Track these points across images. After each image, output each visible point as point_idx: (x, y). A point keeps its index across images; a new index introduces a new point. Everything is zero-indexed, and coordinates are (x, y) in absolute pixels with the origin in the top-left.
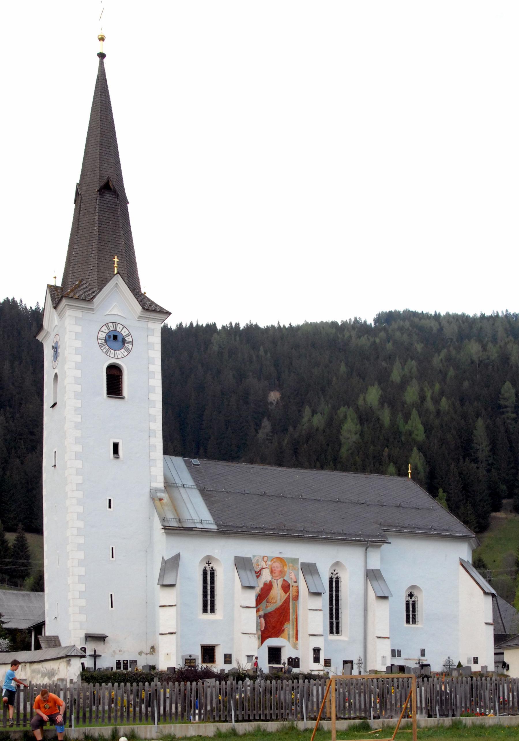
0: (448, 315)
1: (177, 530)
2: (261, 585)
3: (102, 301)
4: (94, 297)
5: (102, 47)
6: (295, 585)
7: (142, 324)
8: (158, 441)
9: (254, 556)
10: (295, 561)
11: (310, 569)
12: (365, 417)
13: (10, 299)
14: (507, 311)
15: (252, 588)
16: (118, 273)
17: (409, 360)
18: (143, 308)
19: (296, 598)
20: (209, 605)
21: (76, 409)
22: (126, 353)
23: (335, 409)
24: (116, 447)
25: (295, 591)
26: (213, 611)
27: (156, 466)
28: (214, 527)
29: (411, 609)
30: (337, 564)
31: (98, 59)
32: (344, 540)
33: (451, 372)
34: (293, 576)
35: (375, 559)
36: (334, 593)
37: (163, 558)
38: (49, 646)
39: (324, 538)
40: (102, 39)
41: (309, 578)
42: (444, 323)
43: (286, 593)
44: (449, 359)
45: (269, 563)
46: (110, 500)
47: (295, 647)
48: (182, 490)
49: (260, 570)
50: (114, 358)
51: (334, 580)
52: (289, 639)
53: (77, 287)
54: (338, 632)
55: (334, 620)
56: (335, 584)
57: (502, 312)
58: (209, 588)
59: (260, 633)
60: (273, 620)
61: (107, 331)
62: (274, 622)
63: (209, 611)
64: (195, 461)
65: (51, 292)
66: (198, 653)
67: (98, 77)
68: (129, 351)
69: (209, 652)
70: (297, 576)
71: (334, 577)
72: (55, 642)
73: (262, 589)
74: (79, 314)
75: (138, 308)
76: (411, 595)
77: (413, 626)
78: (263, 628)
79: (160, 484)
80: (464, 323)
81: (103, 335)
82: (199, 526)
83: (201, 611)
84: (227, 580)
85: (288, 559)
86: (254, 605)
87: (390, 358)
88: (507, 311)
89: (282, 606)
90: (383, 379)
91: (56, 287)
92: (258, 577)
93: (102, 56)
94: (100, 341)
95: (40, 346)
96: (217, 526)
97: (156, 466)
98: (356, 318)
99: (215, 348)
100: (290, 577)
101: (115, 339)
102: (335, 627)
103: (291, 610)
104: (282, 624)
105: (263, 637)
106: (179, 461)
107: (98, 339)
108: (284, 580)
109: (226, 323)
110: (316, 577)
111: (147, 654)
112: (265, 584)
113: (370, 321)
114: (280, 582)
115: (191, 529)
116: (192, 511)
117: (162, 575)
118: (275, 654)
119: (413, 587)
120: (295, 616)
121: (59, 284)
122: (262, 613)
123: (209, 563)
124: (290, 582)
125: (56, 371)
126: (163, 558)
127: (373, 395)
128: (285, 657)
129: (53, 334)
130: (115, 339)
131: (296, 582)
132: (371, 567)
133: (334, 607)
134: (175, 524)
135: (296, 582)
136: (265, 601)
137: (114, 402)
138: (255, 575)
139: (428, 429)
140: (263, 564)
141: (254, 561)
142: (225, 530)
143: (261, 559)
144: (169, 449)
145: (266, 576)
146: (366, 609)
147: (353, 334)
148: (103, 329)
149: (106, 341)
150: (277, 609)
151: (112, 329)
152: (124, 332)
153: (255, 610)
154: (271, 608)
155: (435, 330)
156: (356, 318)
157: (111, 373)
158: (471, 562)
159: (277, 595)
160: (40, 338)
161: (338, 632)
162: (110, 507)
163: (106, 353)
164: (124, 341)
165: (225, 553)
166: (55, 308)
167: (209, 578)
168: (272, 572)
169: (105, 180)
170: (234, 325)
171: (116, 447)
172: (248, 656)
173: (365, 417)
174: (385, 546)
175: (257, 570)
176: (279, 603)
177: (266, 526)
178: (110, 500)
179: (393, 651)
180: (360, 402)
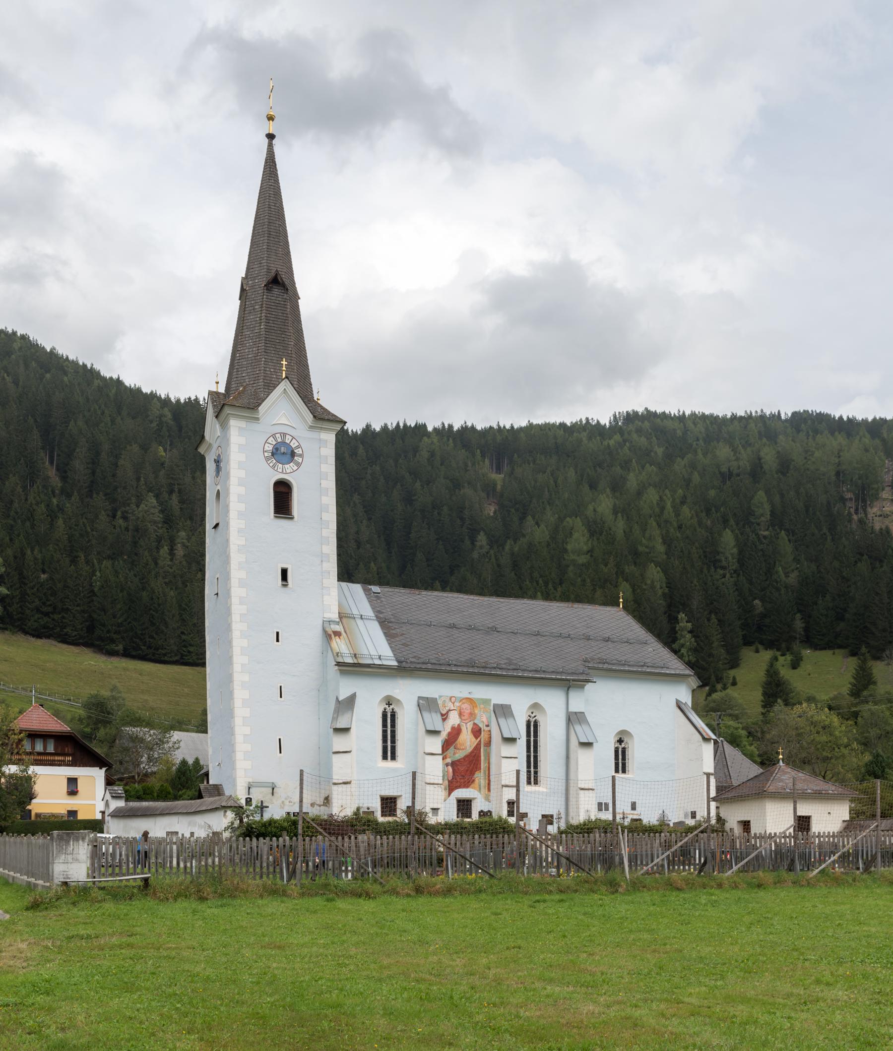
0: (693, 414)
1: (354, 668)
2: (448, 729)
3: (266, 411)
4: (260, 405)
5: (272, 128)
6: (487, 729)
7: (314, 435)
8: (332, 566)
9: (440, 697)
10: (487, 702)
11: (503, 711)
12: (596, 529)
13: (193, 398)
14: (762, 411)
15: (435, 733)
16: (286, 377)
17: (648, 465)
18: (314, 417)
19: (488, 744)
20: (389, 751)
21: (240, 531)
22: (296, 468)
23: (561, 520)
24: (284, 572)
25: (487, 736)
26: (393, 758)
27: (329, 595)
28: (395, 663)
29: (620, 757)
30: (536, 706)
31: (267, 140)
32: (542, 678)
33: (696, 478)
34: (484, 719)
35: (578, 701)
36: (532, 739)
37: (337, 698)
38: (211, 796)
39: (520, 677)
40: (271, 118)
41: (502, 721)
42: (690, 425)
43: (476, 738)
44: (693, 466)
45: (457, 704)
46: (278, 633)
47: (487, 799)
48: (360, 622)
49: (447, 712)
50: (282, 472)
51: (532, 724)
52: (480, 790)
53: (242, 394)
54: (536, 783)
55: (532, 769)
56: (533, 728)
57: (756, 412)
58: (389, 732)
59: (447, 782)
60: (462, 769)
61: (274, 443)
62: (465, 770)
63: (389, 758)
64: (376, 589)
65: (212, 399)
66: (377, 806)
67: (266, 160)
68: (299, 465)
69: (389, 804)
70: (489, 719)
71: (533, 720)
72: (217, 790)
73: (449, 734)
74: (242, 424)
75: (309, 417)
76: (620, 741)
77: (623, 775)
78: (450, 778)
79: (335, 616)
80: (711, 423)
81: (269, 448)
82: (377, 662)
83: (381, 758)
84: (408, 722)
85: (479, 699)
86: (440, 752)
87: (626, 465)
88: (762, 411)
89: (472, 752)
90: (617, 487)
91: (217, 393)
92: (444, 720)
93: (271, 137)
94: (266, 454)
95: (203, 459)
96: (399, 662)
97: (329, 595)
98: (587, 419)
99: (425, 454)
100: (482, 719)
101: (283, 452)
102: (533, 777)
103: (482, 758)
104: (472, 773)
105: (451, 789)
106: (357, 588)
107: (264, 452)
108: (475, 724)
109: (438, 425)
110: (510, 721)
111: (320, 806)
112: (453, 728)
113: (605, 421)
114: (470, 726)
115: (368, 666)
116: (369, 644)
117: (335, 719)
118: (464, 806)
119: (623, 732)
120: (487, 764)
121: (222, 389)
122: (449, 760)
123: (389, 704)
124: (481, 725)
125: (219, 487)
126: (337, 698)
127: (604, 505)
128: (476, 809)
129: (215, 446)
130: (283, 452)
131: (487, 726)
132: (572, 709)
133: (532, 754)
134: (349, 660)
135: (487, 726)
136: (452, 747)
137: (283, 523)
138: (439, 717)
139: (667, 541)
140: (450, 706)
141: (440, 702)
142: (405, 669)
143: (447, 701)
144: (346, 574)
145: (454, 719)
146: (568, 757)
147: (584, 435)
148: (269, 441)
149: (273, 454)
150: (466, 756)
151: (279, 440)
152: (294, 444)
153: (441, 757)
154: (460, 755)
155: (679, 433)
156: (587, 419)
157: (278, 490)
158: (690, 704)
159: (467, 741)
160: (201, 450)
161: (536, 783)
162: (278, 640)
163: (273, 467)
164: (293, 454)
165: (408, 692)
166: (217, 417)
167: (389, 721)
168: (461, 714)
169: (273, 274)
170: (446, 426)
171: (284, 572)
172: (432, 809)
173: (596, 529)
174: (589, 686)
175: (444, 712)
176: (469, 750)
177: (454, 662)
178: (278, 633)
179: (600, 804)
180: (589, 512)
